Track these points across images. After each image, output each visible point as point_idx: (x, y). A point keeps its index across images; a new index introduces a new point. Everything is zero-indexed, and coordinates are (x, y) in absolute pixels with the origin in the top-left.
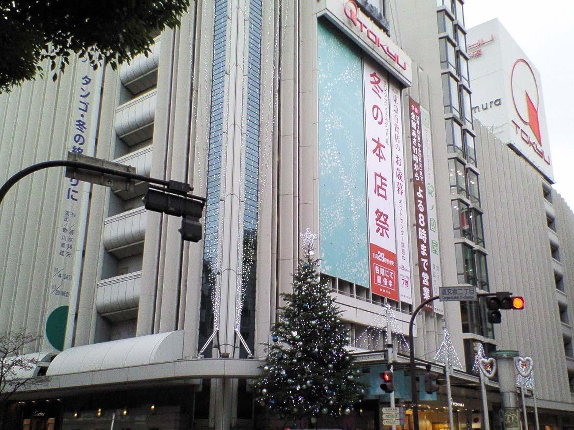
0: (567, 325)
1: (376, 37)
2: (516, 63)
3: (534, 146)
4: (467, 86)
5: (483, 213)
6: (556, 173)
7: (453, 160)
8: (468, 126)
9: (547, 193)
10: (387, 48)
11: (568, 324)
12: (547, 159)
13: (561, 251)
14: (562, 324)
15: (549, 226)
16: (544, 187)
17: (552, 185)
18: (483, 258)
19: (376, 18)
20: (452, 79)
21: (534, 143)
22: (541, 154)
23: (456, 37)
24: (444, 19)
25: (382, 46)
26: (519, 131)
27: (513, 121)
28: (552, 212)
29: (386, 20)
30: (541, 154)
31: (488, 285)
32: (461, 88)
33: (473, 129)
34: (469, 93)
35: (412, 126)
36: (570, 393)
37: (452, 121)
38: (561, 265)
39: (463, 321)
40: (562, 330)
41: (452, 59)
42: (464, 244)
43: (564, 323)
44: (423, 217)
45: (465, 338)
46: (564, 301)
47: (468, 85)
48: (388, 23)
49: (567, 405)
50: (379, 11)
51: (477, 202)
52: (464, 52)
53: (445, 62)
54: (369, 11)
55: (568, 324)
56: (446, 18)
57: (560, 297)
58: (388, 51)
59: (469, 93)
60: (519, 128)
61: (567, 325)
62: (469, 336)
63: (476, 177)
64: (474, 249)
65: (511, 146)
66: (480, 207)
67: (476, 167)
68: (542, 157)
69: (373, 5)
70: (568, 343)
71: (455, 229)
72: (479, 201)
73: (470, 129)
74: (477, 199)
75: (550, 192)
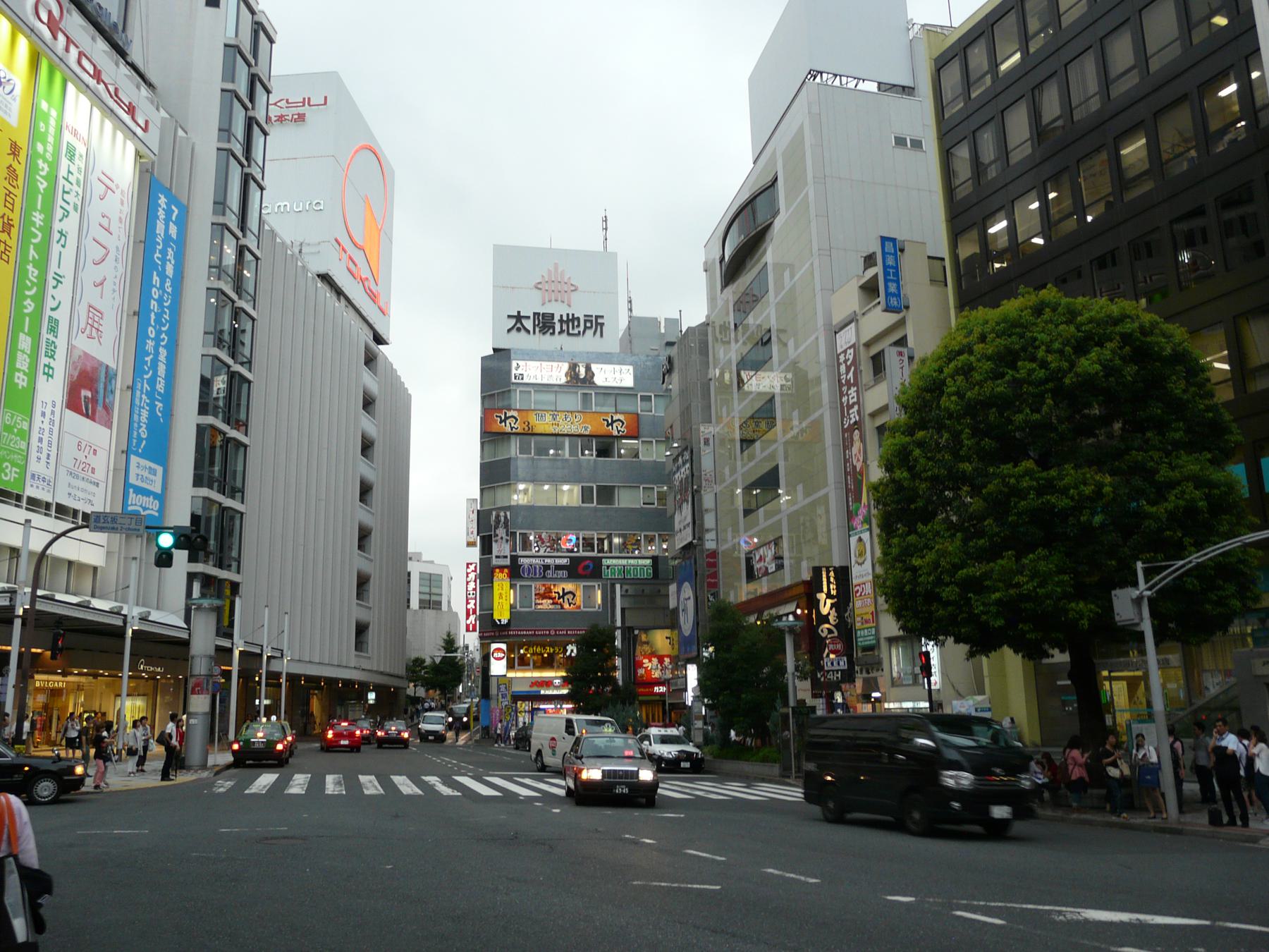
0: (367, 556)
1: (95, 66)
2: (357, 151)
3: (366, 283)
4: (259, 177)
5: (268, 134)
6: (395, 329)
7: (220, 227)
8: (251, 242)
9: (370, 360)
10: (116, 90)
11: (370, 554)
12: (382, 304)
13: (378, 450)
14: (359, 554)
15: (363, 454)
16: (367, 349)
17: (380, 347)
18: (245, 386)
19: (107, 29)
20: (236, 104)
21: (367, 279)
22: (373, 297)
23: (252, 97)
24: (235, 61)
25: (105, 85)
26: (345, 257)
27: (337, 240)
28: (374, 388)
29: (126, 36)
30: (373, 297)
31: (247, 426)
32: (246, 179)
33: (258, 248)
34: (262, 189)
35: (107, 609)
36: (356, 601)
37: (228, 154)
38: (376, 425)
39: (201, 397)
40: (357, 613)
41: (239, 129)
42: (216, 358)
43: (362, 553)
44: (149, 333)
45: (200, 422)
46: (370, 476)
47: (261, 175)
48: (129, 43)
49: (348, 671)
50: (55, 535)
51: (250, 301)
52: (262, 122)
53: (225, 131)
54: (95, 14)
55: (370, 554)
56: (238, 57)
57: (365, 469)
58: (116, 95)
59: (262, 189)
60: (345, 252)
61: (367, 556)
62: (209, 420)
63: (251, 322)
64: (227, 436)
65: (325, 278)
66: (263, 179)
67: (254, 308)
68: (374, 301)
69: (102, 5)
70: (369, 447)
71: (206, 333)
72: (255, 301)
73: (253, 246)
74: (246, 358)
75: (376, 358)
